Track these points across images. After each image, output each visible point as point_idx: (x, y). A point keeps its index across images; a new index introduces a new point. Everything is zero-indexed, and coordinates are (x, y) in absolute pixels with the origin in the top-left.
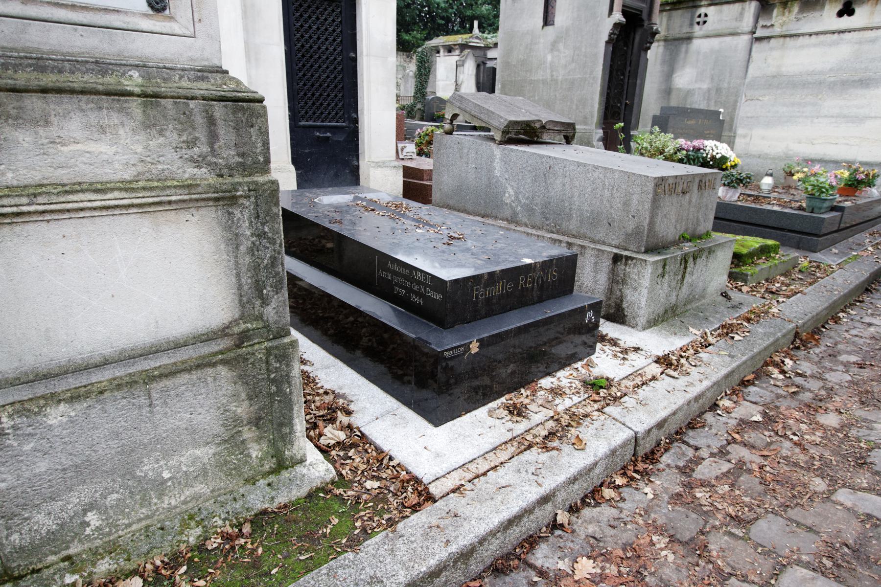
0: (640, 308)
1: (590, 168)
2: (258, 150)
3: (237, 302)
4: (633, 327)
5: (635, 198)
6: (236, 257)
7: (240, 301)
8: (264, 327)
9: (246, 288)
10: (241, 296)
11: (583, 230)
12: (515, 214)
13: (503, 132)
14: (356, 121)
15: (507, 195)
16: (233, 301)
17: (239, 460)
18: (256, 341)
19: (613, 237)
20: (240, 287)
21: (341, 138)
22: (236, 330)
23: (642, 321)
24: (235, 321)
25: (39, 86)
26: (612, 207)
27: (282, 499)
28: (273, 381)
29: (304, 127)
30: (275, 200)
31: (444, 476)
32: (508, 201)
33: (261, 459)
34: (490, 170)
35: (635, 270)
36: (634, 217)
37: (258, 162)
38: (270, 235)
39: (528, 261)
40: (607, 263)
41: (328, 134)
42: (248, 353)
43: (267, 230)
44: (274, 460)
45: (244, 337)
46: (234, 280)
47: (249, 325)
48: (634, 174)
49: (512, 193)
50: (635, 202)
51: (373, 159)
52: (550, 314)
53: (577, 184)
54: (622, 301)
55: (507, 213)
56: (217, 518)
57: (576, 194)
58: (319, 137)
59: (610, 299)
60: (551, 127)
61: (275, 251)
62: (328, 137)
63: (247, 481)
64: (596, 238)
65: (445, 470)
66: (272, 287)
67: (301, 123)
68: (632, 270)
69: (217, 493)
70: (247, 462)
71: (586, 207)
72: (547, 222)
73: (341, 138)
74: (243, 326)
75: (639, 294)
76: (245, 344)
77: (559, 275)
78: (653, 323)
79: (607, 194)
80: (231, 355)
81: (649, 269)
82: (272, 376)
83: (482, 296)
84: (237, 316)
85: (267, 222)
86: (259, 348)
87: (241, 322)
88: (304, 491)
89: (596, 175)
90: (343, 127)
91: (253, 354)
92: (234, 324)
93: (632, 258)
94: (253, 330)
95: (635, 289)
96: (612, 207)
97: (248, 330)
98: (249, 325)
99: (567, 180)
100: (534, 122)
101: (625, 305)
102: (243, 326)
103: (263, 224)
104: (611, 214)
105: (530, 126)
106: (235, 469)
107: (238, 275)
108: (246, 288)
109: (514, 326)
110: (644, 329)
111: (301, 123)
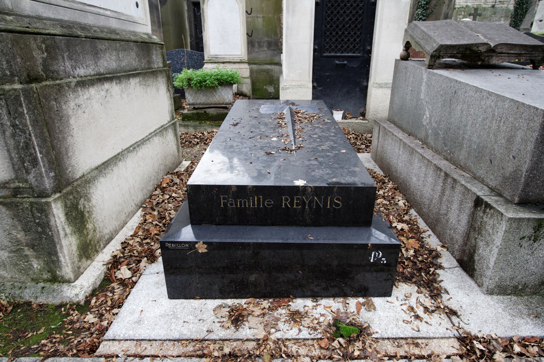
0: (488, 268)
1: (485, 94)
2: (5, 67)
3: (11, 168)
4: (479, 286)
5: (520, 134)
6: (4, 139)
7: (14, 168)
8: (29, 188)
9: (15, 160)
10: (13, 165)
11: (470, 164)
12: (427, 136)
13: (432, 57)
14: (370, 52)
15: (425, 117)
16: (8, 167)
17: (26, 265)
18: (26, 196)
19: (492, 177)
20: (11, 159)
21: (355, 65)
22: (12, 185)
23: (487, 283)
24: (13, 180)
25: (135, 33)
26: (496, 142)
27: (42, 300)
28: (38, 224)
29: (327, 57)
30: (19, 103)
31: (120, 340)
32: (425, 123)
33: (40, 271)
34: (419, 94)
35: (491, 222)
36: (514, 157)
37: (6, 75)
38: (21, 127)
39: (300, 183)
40: (470, 204)
41: (345, 62)
42: (18, 202)
43: (17, 123)
44: (50, 274)
45: (16, 192)
46: (6, 153)
47: (21, 185)
48: (523, 104)
49: (428, 116)
50: (518, 139)
51: (377, 81)
52: (311, 239)
53: (472, 112)
54: (474, 252)
55: (422, 135)
56: (3, 294)
57: (470, 123)
58: (337, 64)
59: (466, 244)
60: (504, 50)
61: (26, 138)
62: (345, 64)
63: (33, 280)
64: (478, 174)
65: (127, 337)
66: (29, 162)
67: (325, 54)
68: (489, 221)
69: (15, 280)
70: (31, 269)
71: (475, 139)
72: (445, 149)
73: (355, 65)
74: (17, 184)
75: (491, 251)
76: (19, 196)
77: (355, 205)
78: (501, 290)
79: (494, 126)
80: (8, 200)
81: (503, 227)
82: (37, 221)
83: (231, 204)
84: (13, 177)
85: (17, 118)
86: (27, 201)
87: (16, 181)
88: (57, 302)
89: (488, 102)
90: (358, 57)
91: (22, 204)
92: (12, 181)
93: (491, 207)
94: (23, 188)
95: (487, 244)
96: (496, 142)
97: (20, 188)
98: (21, 185)
99: (465, 106)
100: (477, 45)
101: (476, 258)
102: (17, 184)
103: (15, 119)
104: (494, 149)
105: (471, 50)
106: (23, 270)
107: (8, 151)
108: (15, 160)
109: (254, 241)
110: (490, 292)
111: (325, 54)
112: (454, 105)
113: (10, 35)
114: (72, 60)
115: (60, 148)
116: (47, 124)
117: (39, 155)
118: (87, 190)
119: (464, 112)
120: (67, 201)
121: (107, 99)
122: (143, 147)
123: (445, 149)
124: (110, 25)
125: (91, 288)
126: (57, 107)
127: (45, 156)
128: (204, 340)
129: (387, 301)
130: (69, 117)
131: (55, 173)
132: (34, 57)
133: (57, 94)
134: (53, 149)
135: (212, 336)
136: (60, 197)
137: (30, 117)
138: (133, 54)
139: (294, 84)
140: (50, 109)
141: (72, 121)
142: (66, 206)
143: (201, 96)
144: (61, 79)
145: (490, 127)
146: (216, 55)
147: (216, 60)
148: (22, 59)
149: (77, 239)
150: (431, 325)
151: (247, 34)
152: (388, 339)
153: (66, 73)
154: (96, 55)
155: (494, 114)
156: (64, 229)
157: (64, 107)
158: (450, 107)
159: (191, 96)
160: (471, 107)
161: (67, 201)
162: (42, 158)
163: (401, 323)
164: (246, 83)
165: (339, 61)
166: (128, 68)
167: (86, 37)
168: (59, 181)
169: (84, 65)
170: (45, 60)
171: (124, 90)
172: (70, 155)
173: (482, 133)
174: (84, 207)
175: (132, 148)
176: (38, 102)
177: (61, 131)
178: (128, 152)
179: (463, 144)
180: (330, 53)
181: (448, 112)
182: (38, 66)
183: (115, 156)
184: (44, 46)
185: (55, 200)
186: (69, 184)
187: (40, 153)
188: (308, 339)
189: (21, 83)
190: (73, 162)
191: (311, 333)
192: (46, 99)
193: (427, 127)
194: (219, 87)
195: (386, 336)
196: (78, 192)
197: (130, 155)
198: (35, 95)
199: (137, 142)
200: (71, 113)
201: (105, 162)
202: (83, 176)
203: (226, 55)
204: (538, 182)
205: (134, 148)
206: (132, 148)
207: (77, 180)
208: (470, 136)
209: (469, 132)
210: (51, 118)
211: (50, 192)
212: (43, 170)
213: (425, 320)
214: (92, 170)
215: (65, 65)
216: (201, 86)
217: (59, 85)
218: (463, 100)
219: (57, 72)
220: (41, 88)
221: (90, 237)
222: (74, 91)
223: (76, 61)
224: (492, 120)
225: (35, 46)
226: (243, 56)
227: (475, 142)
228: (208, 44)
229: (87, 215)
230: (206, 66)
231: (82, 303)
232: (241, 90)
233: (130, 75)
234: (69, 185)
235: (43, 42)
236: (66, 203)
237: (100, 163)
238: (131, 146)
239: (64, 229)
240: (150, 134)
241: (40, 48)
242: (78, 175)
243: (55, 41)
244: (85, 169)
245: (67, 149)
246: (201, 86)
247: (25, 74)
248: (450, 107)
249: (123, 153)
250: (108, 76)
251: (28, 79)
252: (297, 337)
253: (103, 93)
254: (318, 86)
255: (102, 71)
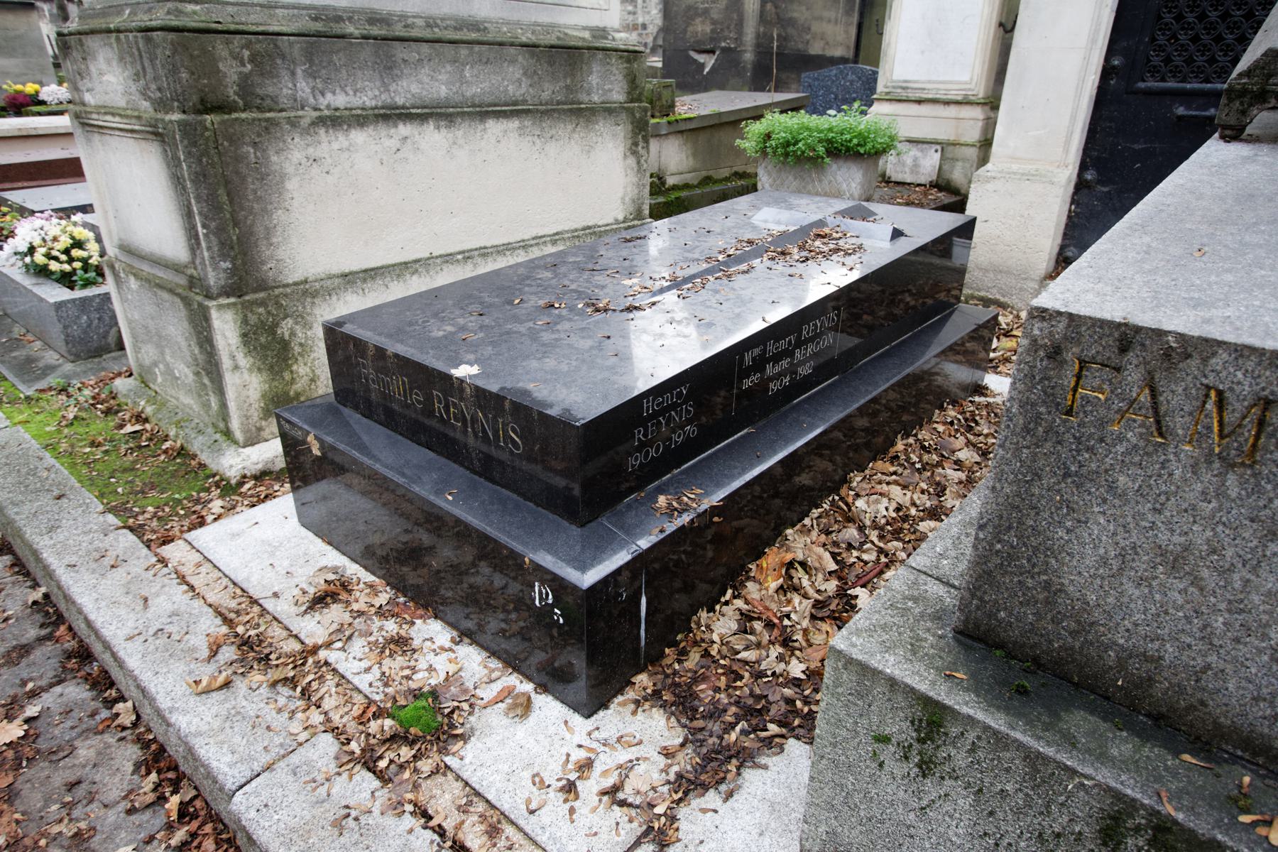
29: (1149, 93)
58: (1180, 118)
67: (1141, 85)
111: (1141, 85)
113: (172, 36)
114: (315, 78)
115: (252, 226)
116: (227, 183)
117: (200, 229)
118: (304, 307)
120: (250, 315)
124: (472, 13)
125: (260, 466)
126: (256, 157)
127: (214, 234)
128: (254, 602)
129: (566, 722)
130: (283, 177)
131: (234, 264)
132: (219, 71)
133: (259, 135)
134: (236, 224)
135: (269, 605)
136: (234, 304)
137: (189, 167)
138: (515, 72)
139: (1015, 167)
140: (238, 159)
141: (292, 185)
142: (245, 321)
143: (791, 178)
144: (282, 110)
146: (906, 81)
147: (904, 95)
148: (193, 73)
149: (265, 382)
150: (573, 822)
151: (1001, 25)
152: (467, 784)
153: (295, 100)
154: (389, 69)
156: (233, 357)
157: (274, 158)
159: (770, 174)
161: (250, 315)
162: (206, 235)
163: (527, 775)
164: (964, 160)
165: (1188, 108)
166: (488, 99)
167: (365, 37)
168: (240, 279)
169: (348, 89)
170: (244, 78)
171: (461, 141)
172: (275, 240)
174: (293, 334)
175: (460, 257)
176: (211, 145)
177: (259, 199)
180: (1163, 80)
182: (226, 86)
183: (406, 263)
184: (246, 53)
185: (220, 307)
186: (263, 286)
187: (204, 226)
188: (360, 692)
189: (184, 112)
190: (281, 253)
191: (375, 684)
192: (231, 141)
194: (827, 160)
195: (465, 776)
196: (278, 305)
198: (207, 134)
199: (485, 248)
200: (290, 169)
201: (372, 269)
202: (306, 281)
203: (929, 82)
204: (1030, 582)
210: (237, 173)
211: (215, 291)
212: (206, 254)
213: (577, 804)
215: (295, 86)
216: (787, 155)
217: (267, 120)
219: (274, 99)
220: (223, 122)
221: (298, 387)
222: (306, 132)
223: (327, 81)
225: (225, 53)
226: (972, 86)
228: (891, 52)
229: (297, 349)
230: (877, 108)
231: (233, 482)
232: (947, 175)
233: (487, 112)
234: (265, 289)
235: (248, 46)
236: (246, 316)
237: (355, 268)
238: (460, 253)
239: (233, 357)
241: (237, 57)
242: (296, 276)
243: (276, 45)
244: (312, 271)
245: (269, 232)
246: (787, 155)
247: (195, 98)
249: (431, 262)
250: (413, 111)
251: (200, 107)
252: (350, 677)
253: (393, 143)
254: (1099, 182)
255: (400, 101)
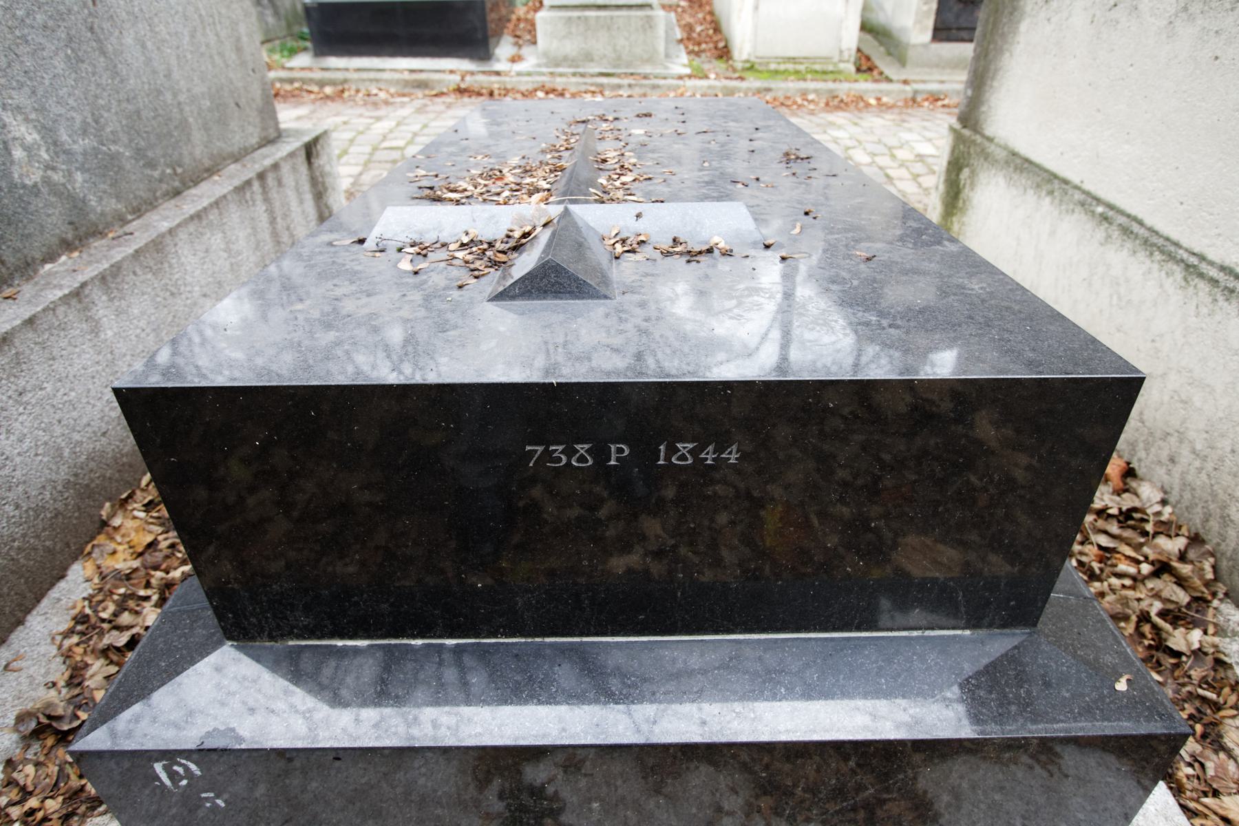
15: (18, 153)
26: (227, 66)
32: (35, 176)
49: (32, 137)
57: (173, 61)
71: (199, 89)
99: (142, 27)
112: (113, 40)
119: (149, 44)
121: (1115, 14)
122: (1142, 255)
123: (156, 174)
141: (1023, 27)
145: (207, 45)
155: (200, 15)
158: (103, 53)
160: (156, 20)
173: (203, 68)
178: (1083, 204)
179: (186, 120)
181: (106, 69)
193: (57, 177)
197: (1079, 216)
205: (1105, 218)
206: (1100, 209)
207: (983, 136)
208: (189, 90)
209: (182, 83)
214: (1005, 148)
218: (128, 13)
224: (204, 28)
227: (203, 94)
240: (1223, 268)
245: (996, 70)
248: (103, 53)
